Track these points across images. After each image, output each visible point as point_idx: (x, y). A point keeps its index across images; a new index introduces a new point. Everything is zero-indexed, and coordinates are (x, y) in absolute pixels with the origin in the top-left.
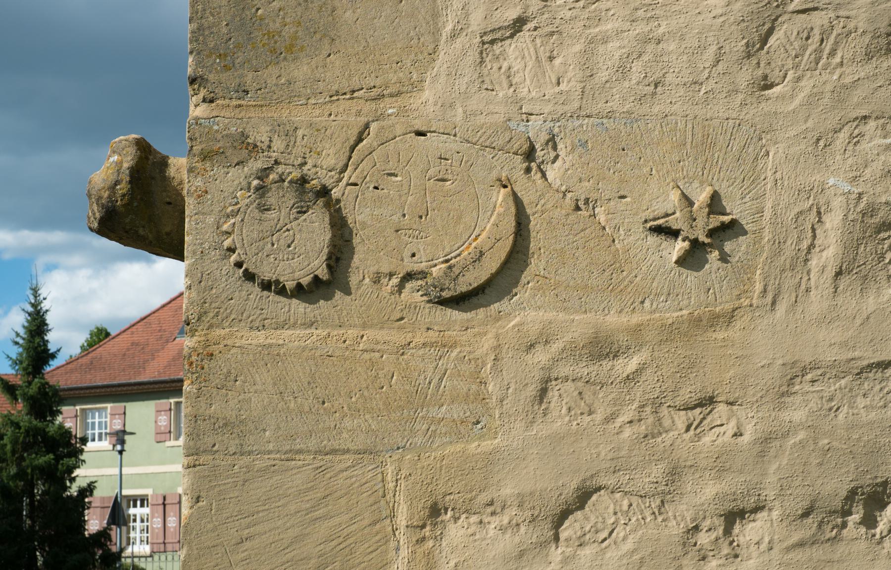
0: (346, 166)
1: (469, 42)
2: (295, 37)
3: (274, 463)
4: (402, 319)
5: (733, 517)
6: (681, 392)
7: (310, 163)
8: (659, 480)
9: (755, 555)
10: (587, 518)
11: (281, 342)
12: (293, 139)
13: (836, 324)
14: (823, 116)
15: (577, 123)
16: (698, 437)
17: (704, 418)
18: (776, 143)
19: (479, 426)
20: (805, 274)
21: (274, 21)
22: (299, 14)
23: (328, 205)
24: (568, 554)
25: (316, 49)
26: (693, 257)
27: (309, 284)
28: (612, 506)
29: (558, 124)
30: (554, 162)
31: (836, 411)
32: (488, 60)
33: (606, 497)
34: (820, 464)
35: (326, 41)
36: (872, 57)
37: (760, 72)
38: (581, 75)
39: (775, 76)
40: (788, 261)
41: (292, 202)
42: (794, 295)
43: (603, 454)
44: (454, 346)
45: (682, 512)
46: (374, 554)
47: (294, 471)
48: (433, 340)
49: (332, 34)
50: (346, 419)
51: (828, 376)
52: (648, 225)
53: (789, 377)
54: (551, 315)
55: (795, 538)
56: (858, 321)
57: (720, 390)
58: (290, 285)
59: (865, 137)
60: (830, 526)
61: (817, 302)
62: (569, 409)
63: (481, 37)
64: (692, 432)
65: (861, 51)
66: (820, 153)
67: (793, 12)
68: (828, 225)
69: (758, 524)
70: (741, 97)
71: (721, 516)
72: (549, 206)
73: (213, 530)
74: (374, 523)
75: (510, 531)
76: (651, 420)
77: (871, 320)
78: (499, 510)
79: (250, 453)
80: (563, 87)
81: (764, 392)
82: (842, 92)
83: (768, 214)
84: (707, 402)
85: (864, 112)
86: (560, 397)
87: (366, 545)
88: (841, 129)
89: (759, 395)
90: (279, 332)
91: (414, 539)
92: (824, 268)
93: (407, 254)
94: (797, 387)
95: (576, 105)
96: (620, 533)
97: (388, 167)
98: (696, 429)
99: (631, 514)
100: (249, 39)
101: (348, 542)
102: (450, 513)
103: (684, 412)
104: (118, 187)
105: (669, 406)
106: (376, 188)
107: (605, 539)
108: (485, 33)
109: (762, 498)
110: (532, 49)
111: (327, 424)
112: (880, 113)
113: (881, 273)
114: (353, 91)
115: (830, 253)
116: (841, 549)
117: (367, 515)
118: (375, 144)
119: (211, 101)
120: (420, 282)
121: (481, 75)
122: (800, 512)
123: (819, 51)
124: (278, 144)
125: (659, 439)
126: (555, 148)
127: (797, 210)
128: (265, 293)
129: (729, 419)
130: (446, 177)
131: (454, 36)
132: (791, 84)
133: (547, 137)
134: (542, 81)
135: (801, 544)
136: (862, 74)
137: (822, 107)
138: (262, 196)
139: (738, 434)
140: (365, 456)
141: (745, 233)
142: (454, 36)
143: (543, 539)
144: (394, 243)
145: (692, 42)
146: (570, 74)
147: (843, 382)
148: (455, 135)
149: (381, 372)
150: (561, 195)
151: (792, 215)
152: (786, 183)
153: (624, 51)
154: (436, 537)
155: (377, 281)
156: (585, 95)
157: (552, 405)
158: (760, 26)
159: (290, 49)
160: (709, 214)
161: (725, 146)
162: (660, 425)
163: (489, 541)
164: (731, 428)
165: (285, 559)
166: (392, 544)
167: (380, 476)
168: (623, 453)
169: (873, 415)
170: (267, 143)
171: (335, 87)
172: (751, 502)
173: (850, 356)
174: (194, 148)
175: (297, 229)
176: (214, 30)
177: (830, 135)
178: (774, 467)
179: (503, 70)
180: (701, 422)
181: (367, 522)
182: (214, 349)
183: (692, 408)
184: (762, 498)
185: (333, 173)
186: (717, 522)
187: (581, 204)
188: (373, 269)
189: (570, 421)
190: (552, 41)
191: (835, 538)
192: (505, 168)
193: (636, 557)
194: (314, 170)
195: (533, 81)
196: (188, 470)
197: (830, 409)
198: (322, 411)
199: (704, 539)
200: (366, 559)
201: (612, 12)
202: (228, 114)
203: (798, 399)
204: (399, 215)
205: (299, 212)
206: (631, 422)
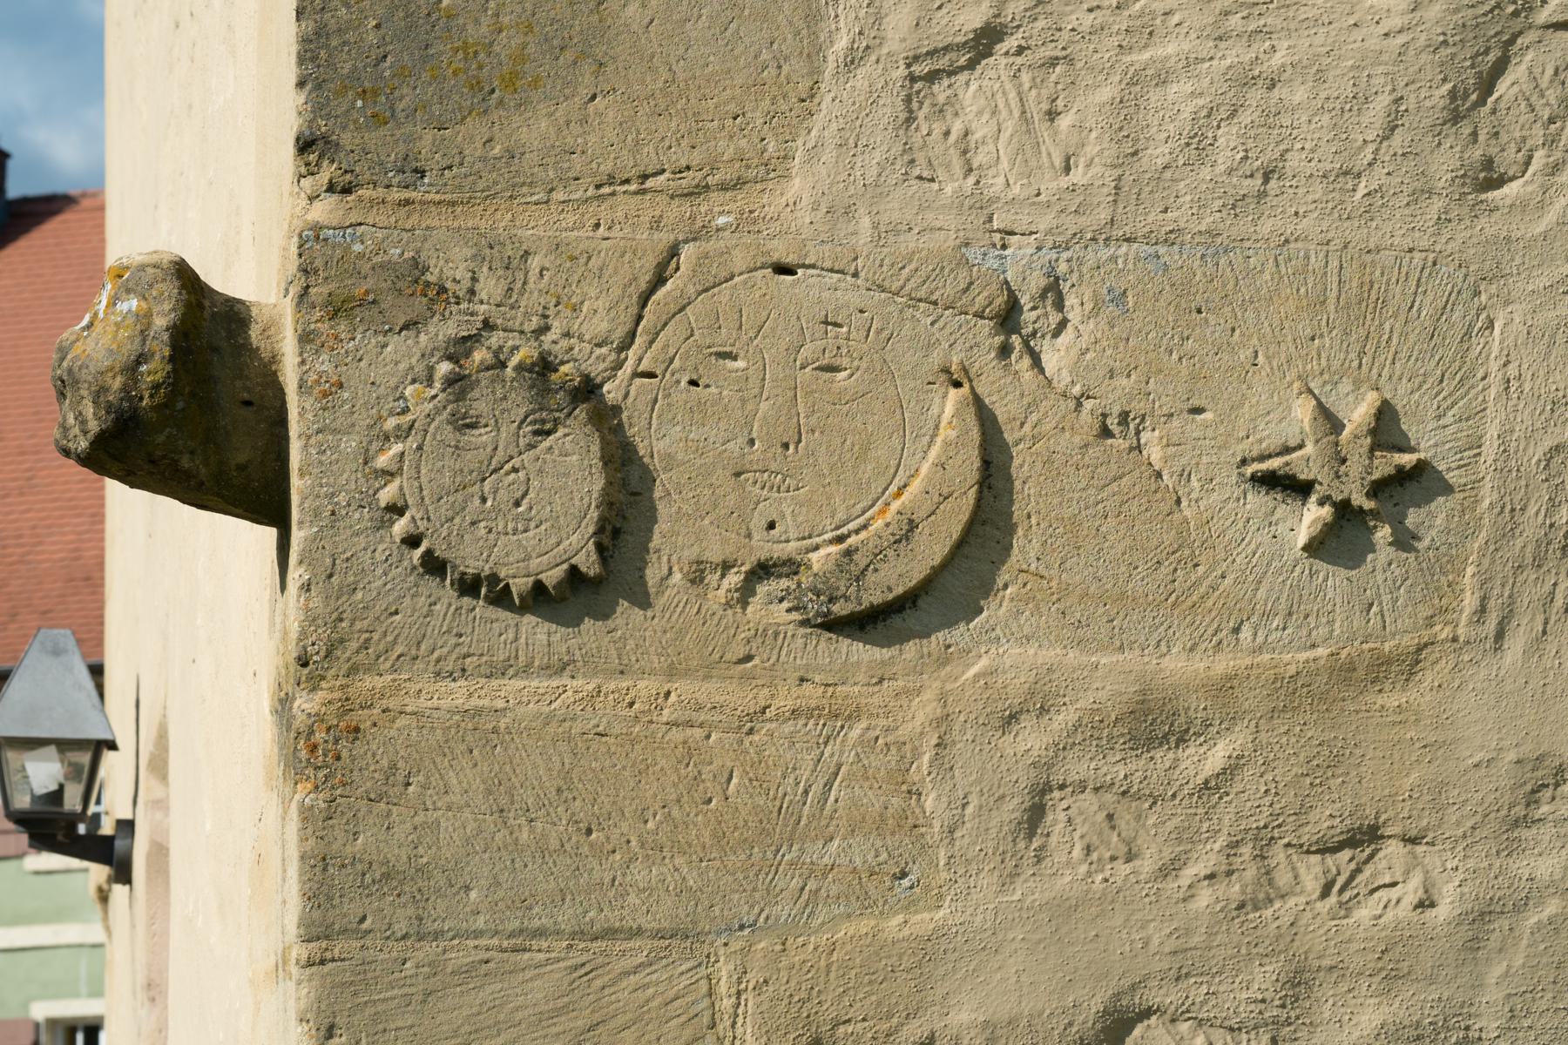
0: (632, 335)
1: (882, 77)
2: (521, 57)
3: (487, 956)
4: (748, 658)
6: (1313, 816)
8: (1268, 995)
11: (500, 704)
12: (520, 276)
15: (1105, 254)
16: (1346, 908)
17: (1358, 870)
18: (1507, 303)
19: (906, 882)
26: (1342, 537)
29: (1065, 255)
30: (1057, 333)
32: (921, 115)
33: (1161, 1030)
35: (587, 68)
37: (1477, 153)
39: (1508, 160)
41: (522, 411)
42: (1540, 619)
43: (1156, 941)
44: (854, 716)
47: (529, 974)
49: (599, 51)
52: (1249, 470)
53: (1529, 787)
54: (1050, 655)
57: (1391, 813)
58: (519, 586)
62: (1088, 850)
63: (908, 66)
64: (1333, 899)
67: (1547, 27)
70: (1437, 204)
72: (1047, 427)
76: (1251, 873)
79: (437, 935)
80: (1078, 176)
81: (1478, 818)
83: (1490, 450)
84: (1365, 837)
89: (1469, 824)
90: (495, 683)
93: (758, 523)
94: (1545, 809)
95: (1104, 215)
98: (1341, 891)
100: (425, 59)
103: (1318, 857)
104: (144, 368)
105: (1288, 845)
106: (693, 383)
108: (916, 58)
109: (1473, 1034)
110: (1012, 95)
111: (596, 875)
114: (645, 177)
118: (691, 290)
119: (347, 190)
124: (490, 287)
125: (1268, 913)
126: (1059, 305)
127: (1548, 443)
129: (1407, 872)
130: (837, 362)
131: (851, 62)
132: (1539, 179)
133: (1043, 282)
134: (1033, 163)
138: (460, 397)
139: (1426, 904)
140: (674, 942)
141: (1448, 489)
142: (851, 62)
146: (1091, 150)
148: (855, 275)
150: (1072, 404)
153: (1201, 102)
155: (696, 578)
157: (1054, 839)
158: (1478, 54)
159: (511, 81)
160: (1372, 450)
162: (1271, 882)
164: (1411, 891)
168: (1196, 940)
170: (466, 284)
171: (607, 167)
174: (312, 291)
175: (533, 469)
176: (350, 36)
178: (1498, 970)
179: (953, 138)
180: (1352, 878)
182: (362, 717)
185: (604, 350)
187: (1112, 423)
188: (691, 554)
190: (1053, 78)
192: (958, 347)
194: (564, 343)
196: (308, 971)
198: (585, 850)
201: (1176, 19)
203: (1546, 832)
205: (536, 433)
206: (1211, 876)
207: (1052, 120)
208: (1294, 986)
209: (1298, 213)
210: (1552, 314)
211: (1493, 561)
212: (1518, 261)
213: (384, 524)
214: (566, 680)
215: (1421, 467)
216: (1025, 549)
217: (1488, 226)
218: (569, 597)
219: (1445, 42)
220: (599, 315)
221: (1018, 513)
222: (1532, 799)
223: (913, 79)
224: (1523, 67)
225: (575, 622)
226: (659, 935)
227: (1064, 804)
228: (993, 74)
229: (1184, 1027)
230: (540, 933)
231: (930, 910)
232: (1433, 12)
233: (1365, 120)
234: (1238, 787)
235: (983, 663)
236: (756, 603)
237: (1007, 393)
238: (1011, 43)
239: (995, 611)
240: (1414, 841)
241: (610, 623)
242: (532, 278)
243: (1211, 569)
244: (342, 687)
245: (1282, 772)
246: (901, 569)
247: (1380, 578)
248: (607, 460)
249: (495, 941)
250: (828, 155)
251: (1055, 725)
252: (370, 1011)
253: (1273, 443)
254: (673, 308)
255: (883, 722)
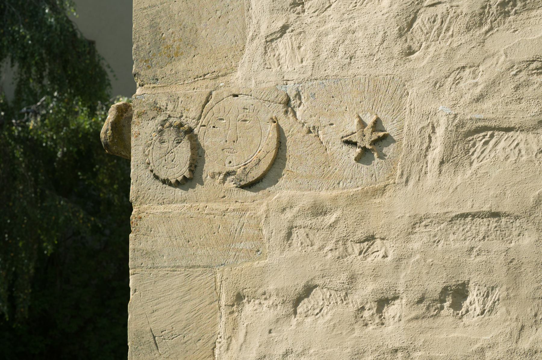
0: (201, 116)
1: (260, 41)
2: (179, 48)
3: (167, 272)
4: (224, 197)
5: (383, 303)
6: (357, 233)
7: (184, 115)
8: (345, 282)
9: (392, 323)
10: (309, 302)
11: (170, 210)
12: (177, 103)
13: (440, 192)
14: (440, 69)
15: (310, 84)
16: (365, 258)
17: (369, 247)
18: (412, 87)
19: (259, 253)
20: (425, 163)
21: (170, 40)
22: (181, 34)
23: (190, 139)
24: (299, 321)
25: (188, 53)
26: (365, 156)
27: (181, 180)
28: (322, 295)
29: (301, 85)
30: (299, 107)
31: (438, 242)
32: (268, 51)
33: (319, 291)
34: (428, 273)
35: (193, 48)
36: (471, 29)
37: (406, 45)
38: (313, 56)
39: (415, 47)
40: (415, 157)
41: (174, 138)
42: (418, 176)
43: (317, 267)
44: (247, 210)
45: (356, 298)
46: (211, 319)
47: (176, 277)
48: (238, 207)
49: (196, 44)
50: (199, 250)
51: (434, 222)
52: (343, 140)
53: (412, 224)
54: (293, 192)
55: (413, 315)
56: (451, 190)
57: (377, 232)
58: (173, 181)
59: (463, 79)
60: (434, 308)
61: (430, 180)
62: (302, 243)
63: (266, 38)
64: (362, 255)
65: (463, 26)
66: (436, 91)
67: (427, 6)
68: (438, 134)
69: (396, 306)
70: (395, 61)
71: (376, 302)
72: (295, 132)
73: (141, 306)
74: (211, 303)
75: (273, 308)
76: (341, 249)
77: (458, 189)
78: (268, 297)
79: (157, 267)
80: (304, 64)
81: (399, 232)
82: (451, 53)
83: (405, 130)
84: (371, 238)
85: (462, 64)
86: (298, 236)
87: (207, 315)
88: (449, 76)
89: (397, 234)
90: (170, 205)
91: (228, 312)
92: (434, 159)
93: (227, 162)
94: (417, 229)
95: (310, 73)
96: (325, 310)
97: (219, 115)
98: (364, 253)
99: (330, 300)
100: (159, 51)
101: (200, 312)
102: (246, 298)
103: (359, 244)
105: (351, 241)
106: (214, 127)
107: (317, 314)
108: (268, 36)
109: (397, 292)
110: (290, 43)
111: (190, 252)
112: (472, 64)
113: (466, 161)
114: (205, 75)
115: (437, 151)
116: (439, 321)
117: (207, 299)
118: (214, 103)
119: (142, 86)
120: (233, 177)
121: (264, 61)
122: (416, 300)
123: (440, 29)
124: (170, 107)
125: (345, 259)
126: (300, 99)
127: (421, 126)
128: (164, 185)
130: (246, 119)
132: (423, 50)
133: (295, 93)
134: (294, 61)
135: (416, 318)
136: (463, 41)
137: (439, 63)
138: (161, 135)
139: (385, 256)
140: (207, 269)
141: (394, 141)
142: (252, 40)
143: (288, 313)
144: (221, 157)
145: (371, 31)
146: (308, 56)
147: (442, 226)
148: (251, 95)
149: (214, 225)
150: (301, 125)
151: (418, 130)
152: (416, 111)
153: (335, 39)
154: (239, 311)
155: (213, 177)
156: (315, 67)
157: (294, 241)
158: (407, 17)
159: (177, 54)
160: (372, 133)
161: (385, 91)
162: (346, 251)
163: (263, 314)
164: (381, 253)
165: (172, 321)
166: (219, 314)
167: (214, 279)
168: (327, 267)
169: (457, 245)
170: (165, 106)
171: (196, 74)
172: (390, 295)
173: (445, 211)
175: (176, 152)
176: (144, 47)
177: (443, 80)
178: (403, 274)
179: (276, 56)
180: (367, 249)
181: (207, 303)
182: (142, 215)
183: (363, 242)
184: (397, 292)
185: (194, 120)
186: (373, 305)
187: (311, 129)
188: (211, 171)
189: (302, 250)
190: (300, 37)
191: (436, 315)
192: (275, 112)
193: (332, 323)
194: (186, 119)
195: (291, 63)
197: (434, 242)
198: (188, 246)
199: (366, 314)
200: (207, 322)
201: (331, 17)
202: (149, 92)
203: (418, 235)
204: (224, 141)
205: (177, 143)
206: (331, 250)
207: (299, 49)
208: (352, 279)
209: (360, 67)
210: (424, 89)
211: (405, 161)
212: (416, 75)
213: (147, 168)
214: (185, 204)
215: (385, 137)
216: (289, 164)
217: (408, 65)
218: (184, 183)
219: (398, 15)
220: (193, 113)
221: (287, 155)
222: (414, 227)
223: (267, 42)
224: (420, 19)
225: (187, 190)
226: (204, 267)
227: (296, 232)
228: (286, 38)
229: (325, 290)
230: (178, 267)
231: (264, 260)
232: (395, 7)
233: (376, 40)
234: (338, 226)
235: (278, 195)
236: (227, 182)
237: (285, 123)
238: (290, 29)
239: (281, 182)
240: (383, 239)
241: (194, 190)
242: (179, 103)
243: (333, 167)
244: (139, 208)
245: (350, 222)
246: (257, 172)
247: (375, 167)
248: (192, 149)
249: (169, 269)
250: (246, 65)
251: (294, 211)
252: (143, 286)
253: (349, 132)
254: (210, 108)
255: (253, 212)
